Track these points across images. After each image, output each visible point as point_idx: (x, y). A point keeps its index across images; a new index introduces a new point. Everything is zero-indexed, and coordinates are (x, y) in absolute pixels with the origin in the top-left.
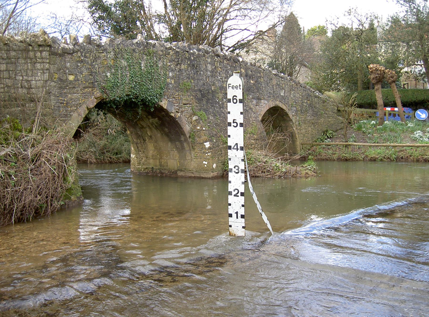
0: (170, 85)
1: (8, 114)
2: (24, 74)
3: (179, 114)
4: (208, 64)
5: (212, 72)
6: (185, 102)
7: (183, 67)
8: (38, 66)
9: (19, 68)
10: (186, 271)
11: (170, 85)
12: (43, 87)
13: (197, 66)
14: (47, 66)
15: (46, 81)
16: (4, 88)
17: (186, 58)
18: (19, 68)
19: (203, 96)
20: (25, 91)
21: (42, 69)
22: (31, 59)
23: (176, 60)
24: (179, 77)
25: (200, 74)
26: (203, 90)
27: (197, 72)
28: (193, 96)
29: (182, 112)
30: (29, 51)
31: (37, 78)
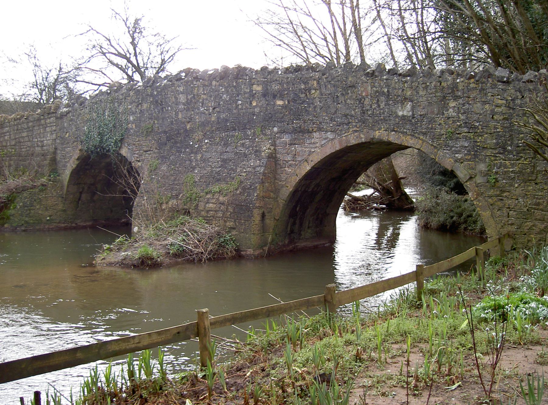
0: (131, 131)
1: (22, 165)
2: (38, 137)
3: (139, 164)
4: (179, 94)
5: (188, 103)
6: (145, 149)
7: (145, 106)
8: (48, 129)
9: (35, 133)
10: (70, 330)
11: (131, 131)
12: (52, 144)
13: (162, 102)
14: (54, 128)
15: (55, 140)
16: (26, 148)
17: (148, 95)
18: (35, 133)
19: (169, 139)
20: (39, 149)
21: (51, 131)
22: (43, 125)
23: (137, 101)
24: (140, 120)
25: (168, 110)
26: (169, 130)
27: (162, 108)
28: (155, 140)
29: (143, 160)
30: (41, 120)
31: (47, 138)
